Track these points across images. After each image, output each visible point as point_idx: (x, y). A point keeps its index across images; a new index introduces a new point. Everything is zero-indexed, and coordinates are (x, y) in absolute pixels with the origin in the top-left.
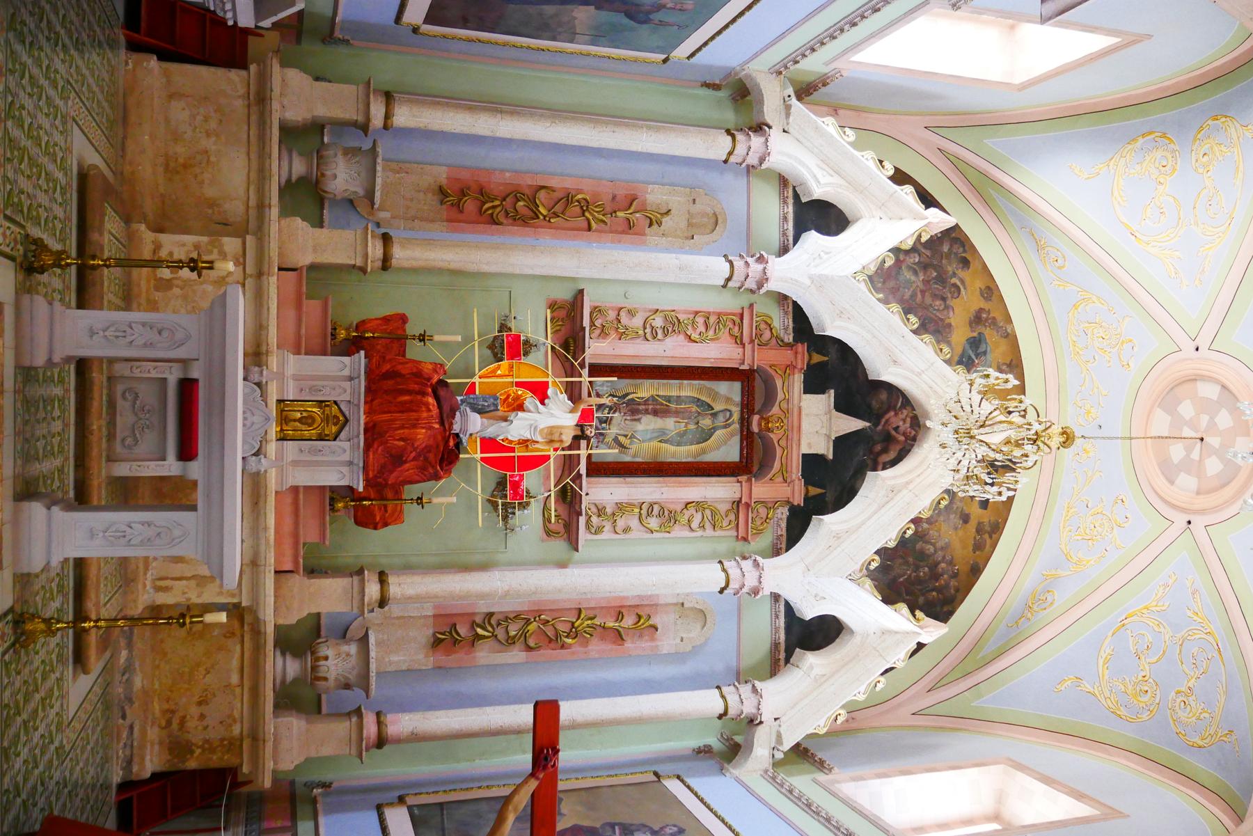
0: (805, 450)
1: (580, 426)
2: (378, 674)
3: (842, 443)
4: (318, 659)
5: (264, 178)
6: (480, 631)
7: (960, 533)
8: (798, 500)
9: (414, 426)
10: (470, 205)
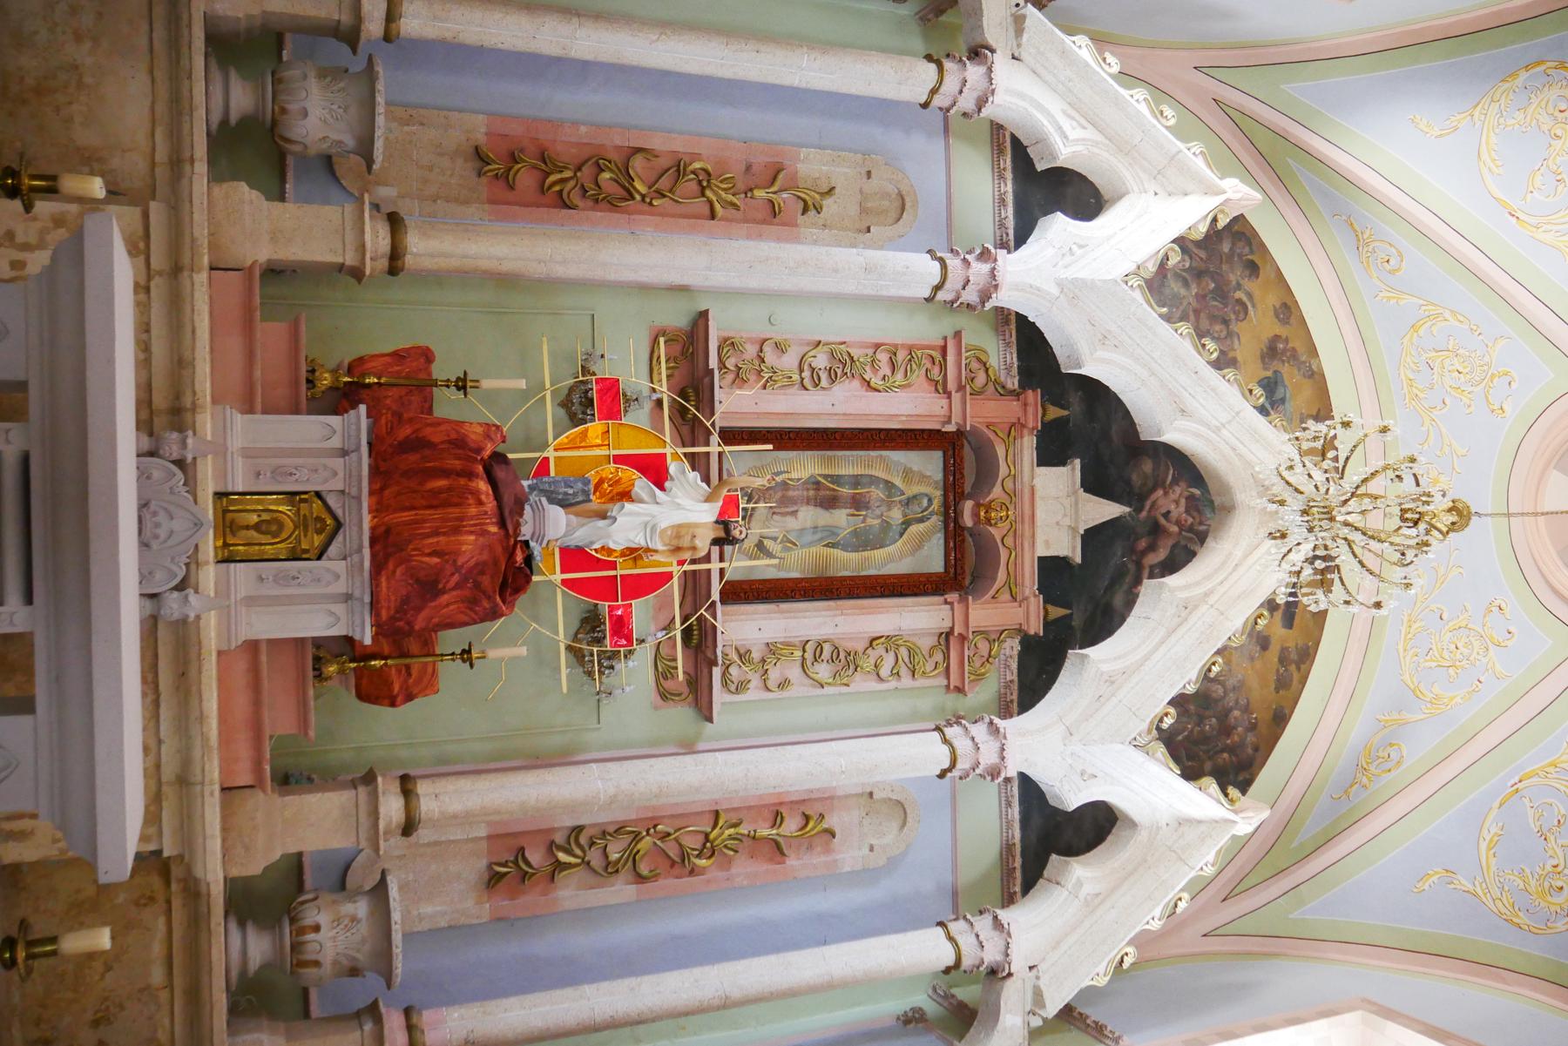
0: (1042, 551)
1: (723, 522)
2: (407, 936)
3: (1094, 538)
4: (302, 931)
5: (180, 114)
6: (562, 856)
7: (1258, 664)
8: (1035, 627)
9: (456, 530)
10: (525, 179)
